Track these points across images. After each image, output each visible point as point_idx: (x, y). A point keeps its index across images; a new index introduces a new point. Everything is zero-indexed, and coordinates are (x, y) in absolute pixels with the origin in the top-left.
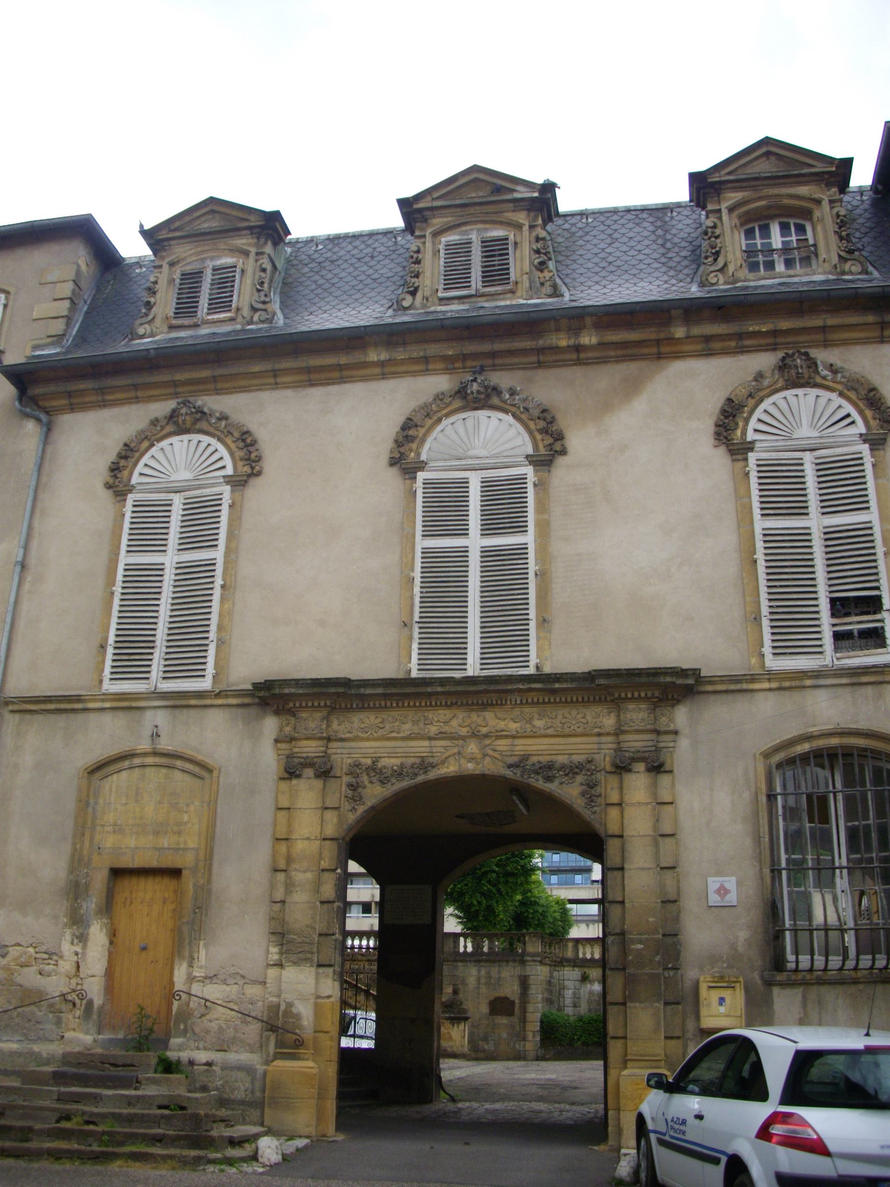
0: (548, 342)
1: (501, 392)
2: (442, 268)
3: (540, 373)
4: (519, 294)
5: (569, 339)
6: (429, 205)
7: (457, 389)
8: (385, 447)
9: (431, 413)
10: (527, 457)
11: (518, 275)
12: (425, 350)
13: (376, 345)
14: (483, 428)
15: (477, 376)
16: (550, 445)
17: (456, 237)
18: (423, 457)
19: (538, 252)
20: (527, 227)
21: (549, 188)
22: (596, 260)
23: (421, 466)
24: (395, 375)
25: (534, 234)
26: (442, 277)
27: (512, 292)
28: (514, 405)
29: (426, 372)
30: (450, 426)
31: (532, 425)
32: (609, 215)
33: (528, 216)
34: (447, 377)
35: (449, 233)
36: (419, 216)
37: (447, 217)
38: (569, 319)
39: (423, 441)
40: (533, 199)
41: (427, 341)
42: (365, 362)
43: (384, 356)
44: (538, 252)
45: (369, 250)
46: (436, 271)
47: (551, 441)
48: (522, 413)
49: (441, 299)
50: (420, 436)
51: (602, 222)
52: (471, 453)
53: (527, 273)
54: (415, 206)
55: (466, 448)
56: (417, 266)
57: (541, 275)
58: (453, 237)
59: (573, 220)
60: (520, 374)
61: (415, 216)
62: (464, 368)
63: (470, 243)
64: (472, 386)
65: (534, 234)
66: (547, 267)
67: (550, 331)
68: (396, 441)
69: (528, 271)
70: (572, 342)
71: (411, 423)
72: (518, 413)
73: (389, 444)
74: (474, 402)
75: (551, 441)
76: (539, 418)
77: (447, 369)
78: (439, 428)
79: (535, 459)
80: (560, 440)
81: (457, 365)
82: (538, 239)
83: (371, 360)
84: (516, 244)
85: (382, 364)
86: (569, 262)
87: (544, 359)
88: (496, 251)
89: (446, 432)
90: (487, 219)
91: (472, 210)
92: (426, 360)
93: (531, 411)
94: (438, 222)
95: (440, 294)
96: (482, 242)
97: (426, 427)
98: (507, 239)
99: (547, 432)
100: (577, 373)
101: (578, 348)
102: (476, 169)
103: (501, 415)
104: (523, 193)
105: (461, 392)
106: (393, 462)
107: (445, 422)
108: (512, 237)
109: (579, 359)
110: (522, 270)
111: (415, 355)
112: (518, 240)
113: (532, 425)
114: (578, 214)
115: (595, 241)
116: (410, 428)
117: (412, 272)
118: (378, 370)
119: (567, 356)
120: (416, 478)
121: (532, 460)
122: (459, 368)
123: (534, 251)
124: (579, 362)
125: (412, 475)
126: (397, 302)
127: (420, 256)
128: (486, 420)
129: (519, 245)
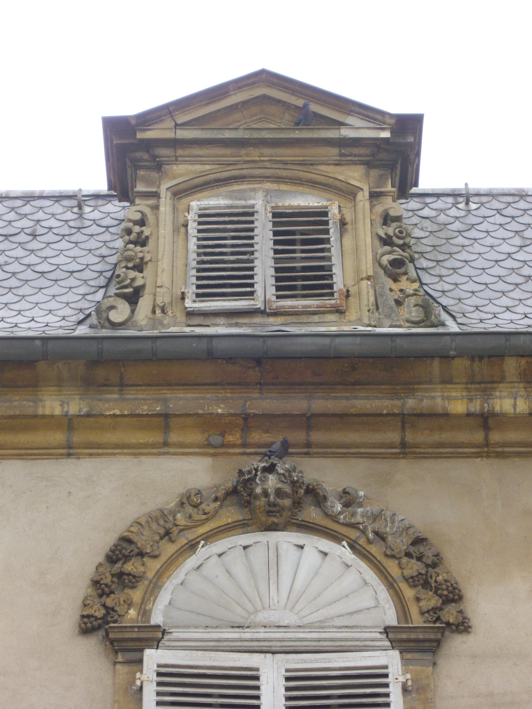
0: (426, 403)
1: (325, 498)
2: (193, 256)
3: (404, 469)
4: (352, 315)
5: (471, 400)
6: (169, 135)
7: (230, 485)
8: (71, 594)
9: (175, 530)
10: (387, 630)
11: (350, 282)
12: (165, 401)
13: (60, 383)
14: (286, 568)
15: (274, 460)
16: (434, 610)
17: (223, 202)
18: (157, 619)
19: (387, 241)
20: (367, 194)
21: (409, 127)
22: (497, 271)
23: (155, 637)
24: (96, 449)
25: (379, 209)
26: (194, 272)
27: (339, 311)
28: (354, 526)
29: (164, 448)
30: (215, 559)
31: (392, 567)
32: (510, 199)
33: (367, 175)
34: (208, 461)
35: (206, 193)
36: (146, 156)
37: (203, 163)
38: (472, 358)
39: (155, 587)
40: (377, 143)
41: (169, 385)
42: (35, 416)
43: (76, 406)
44: (387, 241)
45: (25, 223)
46: (180, 263)
47: (435, 602)
48: (369, 542)
49: (190, 314)
50: (150, 575)
51: (498, 211)
52: (262, 617)
53: (368, 278)
54: (140, 135)
55: (249, 607)
56: (138, 248)
57: (394, 286)
58: (216, 201)
59: (439, 204)
60: (361, 466)
61: (139, 155)
62: (245, 445)
63: (252, 214)
64: (264, 480)
65: (379, 209)
66: (406, 273)
67: (430, 382)
68: (96, 583)
69: (370, 273)
70: (476, 407)
71: (130, 548)
72: (362, 541)
73: (81, 588)
74: (269, 513)
75: (435, 602)
76: (408, 555)
77: (210, 445)
78: (192, 562)
79: (404, 636)
80: (453, 601)
81: (230, 438)
82: (387, 219)
83: (47, 412)
84: (343, 223)
85: (69, 423)
86: (444, 272)
87: (416, 438)
88: (302, 234)
89: (205, 570)
90: (284, 173)
91: (254, 154)
92: (165, 420)
93: (390, 539)
94: (182, 171)
95: (188, 303)
96: (275, 215)
97: (163, 558)
98: (326, 214)
99: (426, 585)
100: (481, 473)
101: (486, 420)
102: (264, 77)
103: (325, 544)
104: (357, 129)
105: (240, 493)
106: (88, 626)
107: (203, 552)
108: (334, 211)
109: (487, 444)
110: (358, 270)
111: (144, 409)
112: (348, 218)
113: (392, 567)
114: (448, 195)
115: (489, 241)
116: (127, 558)
117: (129, 259)
118: (58, 437)
119: (463, 437)
120: (140, 661)
121: (399, 638)
122: (234, 446)
123: (380, 238)
124: (487, 451)
125: (131, 656)
126: (98, 311)
127: (147, 231)
128: (294, 552)
129: (349, 227)
